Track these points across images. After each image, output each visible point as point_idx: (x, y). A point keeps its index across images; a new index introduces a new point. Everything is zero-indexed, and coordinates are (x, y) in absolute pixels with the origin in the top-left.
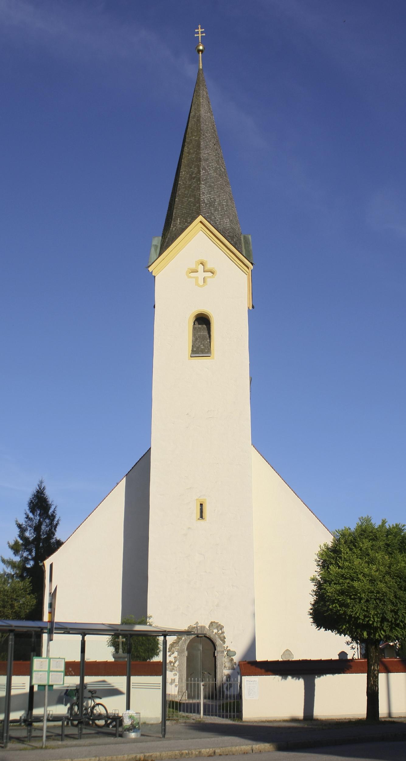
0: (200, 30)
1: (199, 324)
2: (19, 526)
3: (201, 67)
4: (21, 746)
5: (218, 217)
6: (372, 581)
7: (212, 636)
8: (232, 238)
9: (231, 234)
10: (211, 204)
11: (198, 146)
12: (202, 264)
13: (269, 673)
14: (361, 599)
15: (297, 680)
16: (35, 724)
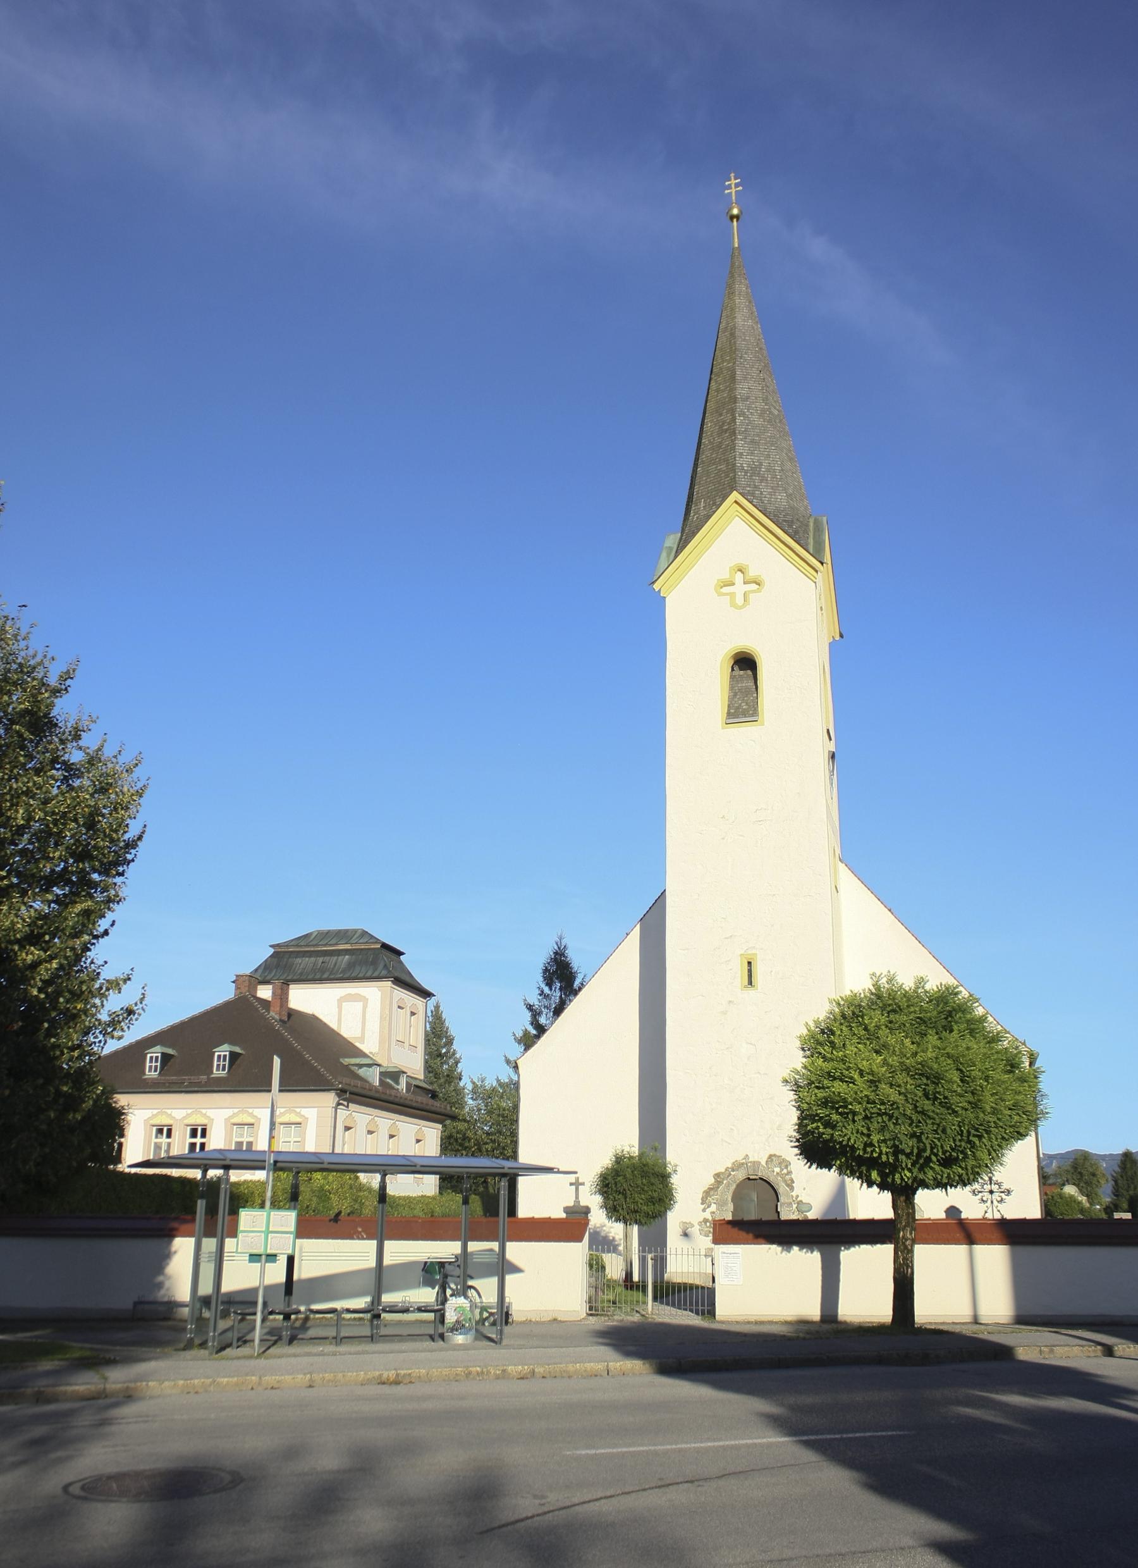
0: (733, 182)
1: (741, 670)
2: (530, 1008)
3: (736, 245)
4: (332, 1348)
5: (766, 491)
6: (874, 1083)
7: (771, 1179)
8: (790, 523)
9: (789, 518)
10: (755, 470)
11: (733, 378)
12: (740, 570)
13: (760, 1240)
14: (854, 1113)
15: (809, 1254)
16: (248, 1317)
